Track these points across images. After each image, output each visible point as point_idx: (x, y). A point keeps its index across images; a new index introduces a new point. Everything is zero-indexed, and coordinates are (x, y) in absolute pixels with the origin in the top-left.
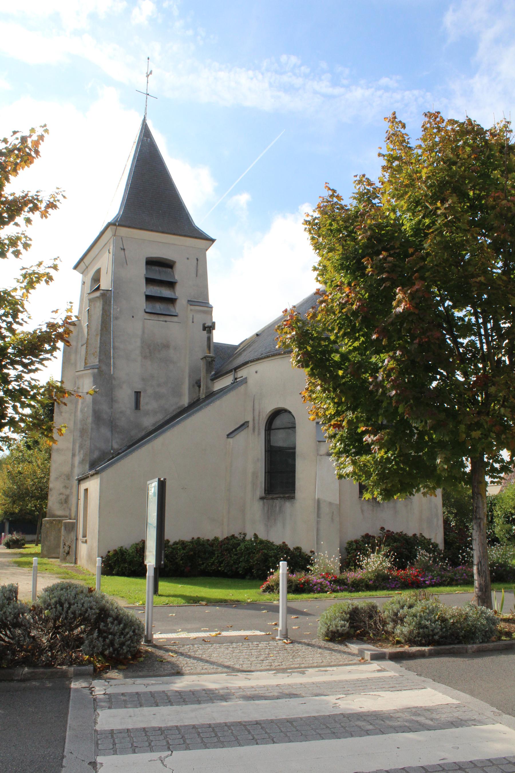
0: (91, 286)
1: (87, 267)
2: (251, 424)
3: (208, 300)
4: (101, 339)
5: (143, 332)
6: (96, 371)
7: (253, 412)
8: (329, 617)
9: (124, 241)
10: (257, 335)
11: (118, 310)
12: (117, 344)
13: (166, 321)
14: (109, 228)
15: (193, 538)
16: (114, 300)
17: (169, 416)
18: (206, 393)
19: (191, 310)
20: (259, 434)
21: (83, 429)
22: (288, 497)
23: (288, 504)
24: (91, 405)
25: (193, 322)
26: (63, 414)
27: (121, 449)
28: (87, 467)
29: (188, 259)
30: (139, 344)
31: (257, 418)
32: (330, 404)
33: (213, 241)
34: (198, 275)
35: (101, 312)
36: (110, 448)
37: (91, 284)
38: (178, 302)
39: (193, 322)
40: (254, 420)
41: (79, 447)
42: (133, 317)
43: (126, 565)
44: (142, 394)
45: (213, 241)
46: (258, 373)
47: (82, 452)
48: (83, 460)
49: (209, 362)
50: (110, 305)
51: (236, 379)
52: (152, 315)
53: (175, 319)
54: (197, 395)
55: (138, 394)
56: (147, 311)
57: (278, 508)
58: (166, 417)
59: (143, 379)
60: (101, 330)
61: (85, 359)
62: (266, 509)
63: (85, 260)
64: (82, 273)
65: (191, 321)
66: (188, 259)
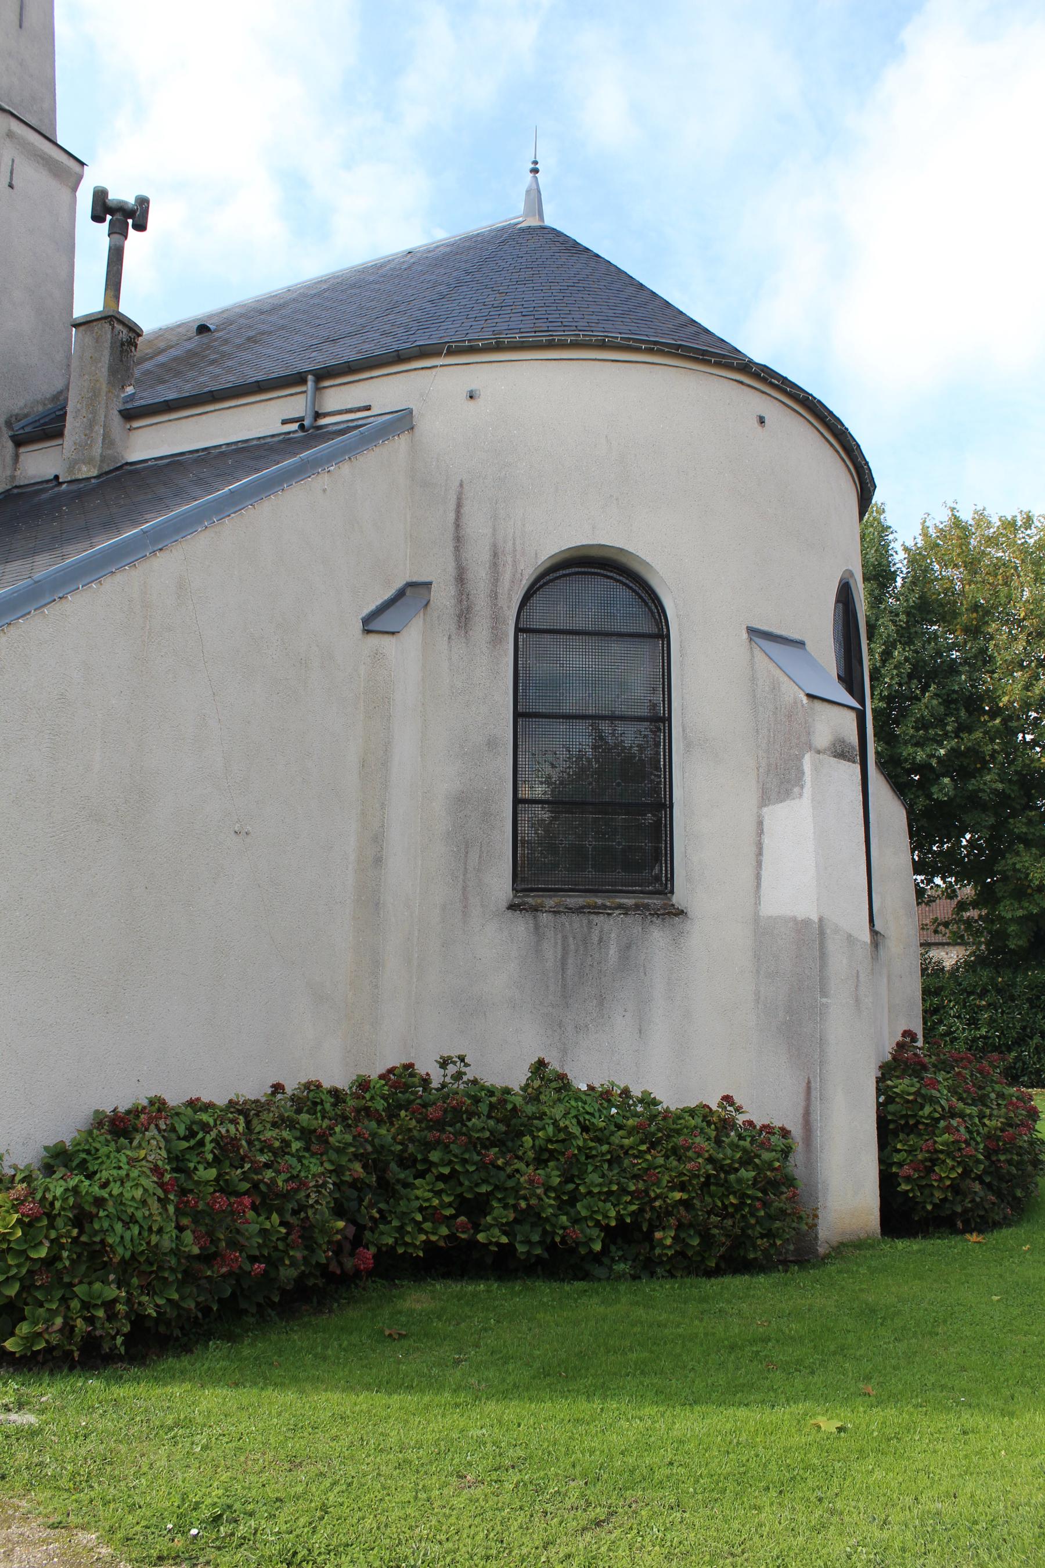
2: (443, 596)
7: (457, 549)
8: (475, 1438)
10: (203, 329)
15: (278, 1088)
18: (103, 458)
19: (10, 135)
20: (496, 639)
22: (637, 907)
23: (658, 936)
25: (11, 186)
31: (479, 575)
34: (25, 24)
40: (461, 578)
43: (112, 1292)
46: (480, 402)
51: (317, 415)
54: (8, 473)
57: (613, 951)
62: (551, 952)
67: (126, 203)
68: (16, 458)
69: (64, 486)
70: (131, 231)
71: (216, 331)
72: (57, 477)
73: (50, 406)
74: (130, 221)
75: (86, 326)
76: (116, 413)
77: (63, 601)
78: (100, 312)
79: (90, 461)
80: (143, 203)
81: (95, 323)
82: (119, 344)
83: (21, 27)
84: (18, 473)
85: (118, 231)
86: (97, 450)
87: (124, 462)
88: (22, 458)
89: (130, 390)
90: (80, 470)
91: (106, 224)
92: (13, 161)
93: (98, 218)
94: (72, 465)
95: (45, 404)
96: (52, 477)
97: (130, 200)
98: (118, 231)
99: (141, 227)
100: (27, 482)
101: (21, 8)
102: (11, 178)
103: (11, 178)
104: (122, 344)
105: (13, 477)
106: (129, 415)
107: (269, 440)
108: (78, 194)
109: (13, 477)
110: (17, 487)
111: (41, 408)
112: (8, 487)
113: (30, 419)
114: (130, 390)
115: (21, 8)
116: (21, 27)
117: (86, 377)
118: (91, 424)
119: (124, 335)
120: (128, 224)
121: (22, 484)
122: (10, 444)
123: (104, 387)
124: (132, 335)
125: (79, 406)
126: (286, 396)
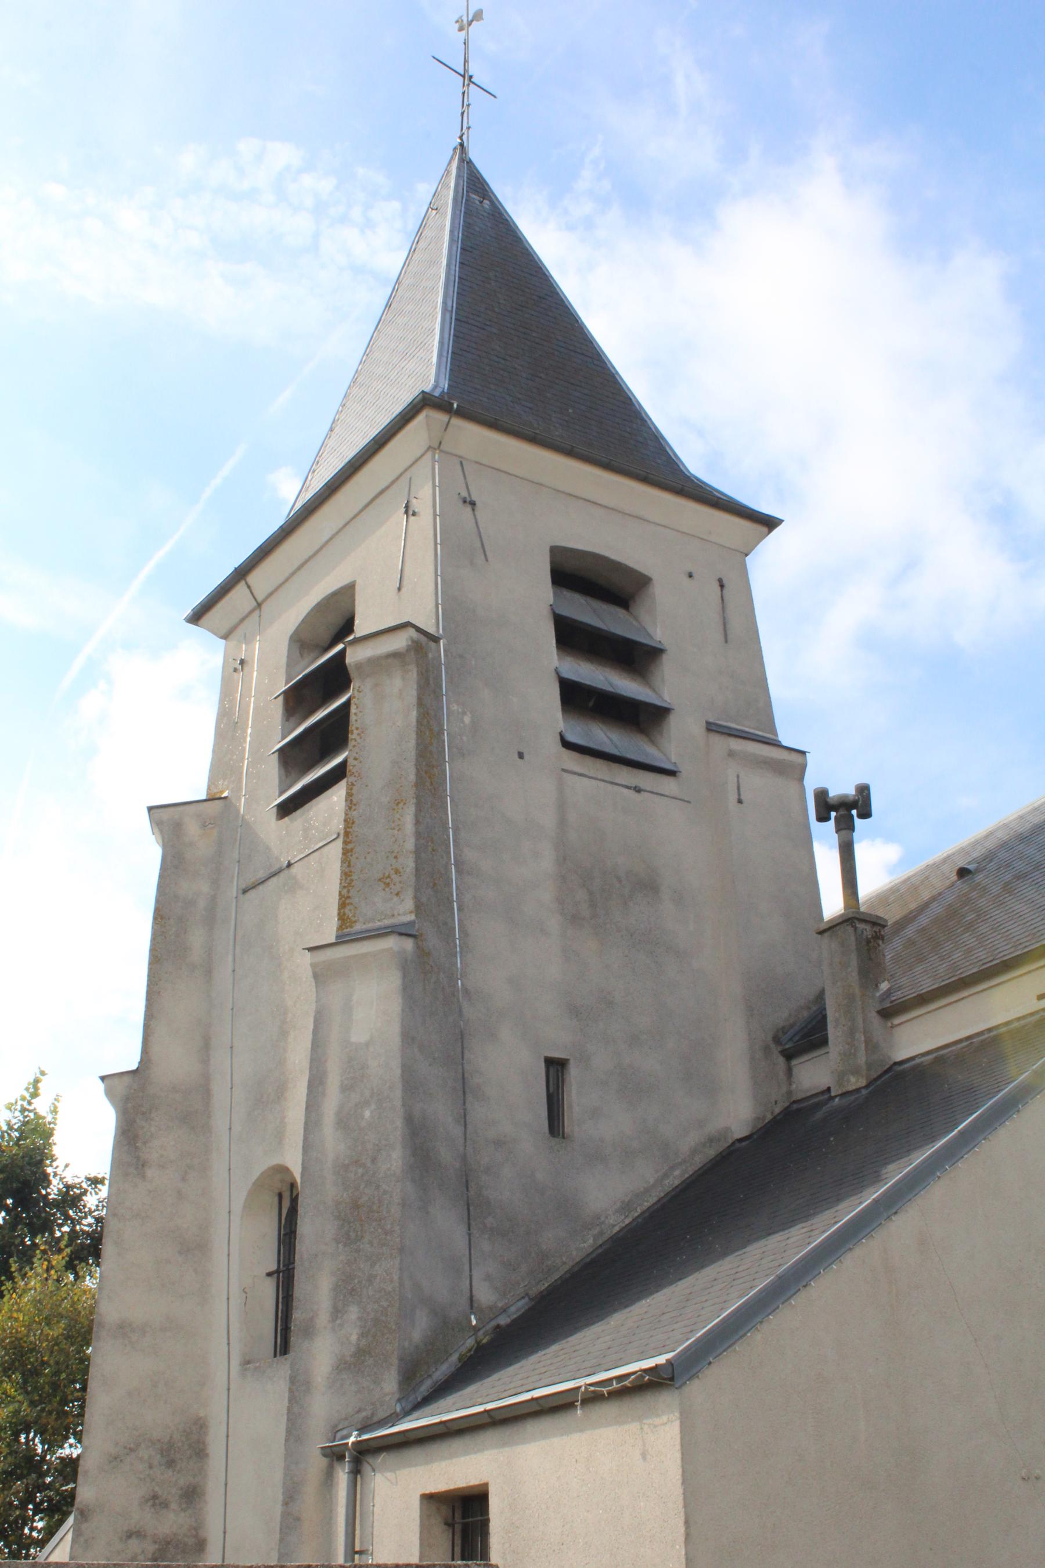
0: (288, 665)
1: (259, 605)
3: (774, 732)
4: (417, 822)
5: (562, 822)
6: (409, 944)
9: (469, 479)
10: (963, 873)
11: (467, 719)
12: (470, 855)
13: (638, 790)
14: (421, 418)
16: (450, 680)
17: (677, 1173)
18: (869, 1066)
19: (731, 754)
21: (356, 1206)
24: (398, 1093)
25: (740, 801)
26: (149, 1173)
27: (504, 1310)
28: (390, 1384)
29: (690, 576)
30: (547, 863)
32: (21, 1403)
33: (770, 523)
34: (730, 637)
35: (414, 714)
36: (464, 1301)
37: (289, 657)
38: (673, 722)
39: (740, 801)
41: (336, 1289)
42: (521, 755)
44: (573, 1073)
45: (770, 523)
47: (353, 1313)
48: (361, 1353)
49: (868, 942)
50: (438, 696)
52: (589, 760)
53: (667, 784)
54: (784, 1089)
55: (556, 1067)
56: (571, 738)
58: (666, 1175)
59: (575, 1011)
60: (416, 785)
61: (343, 904)
63: (253, 578)
64: (225, 637)
65: (733, 798)
66: (690, 576)
67: (846, 796)
68: (789, 1071)
69: (837, 1100)
70: (858, 822)
71: (978, 871)
72: (829, 1089)
73: (814, 1008)
74: (854, 812)
75: (831, 931)
76: (874, 1014)
77: (808, 1288)
78: (841, 916)
79: (856, 1072)
80: (864, 791)
81: (838, 927)
82: (864, 943)
83: (726, 641)
84: (794, 1086)
85: (845, 826)
86: (862, 1059)
87: (891, 1063)
88: (795, 1071)
89: (884, 986)
90: (848, 1081)
91: (832, 822)
92: (738, 777)
93: (822, 818)
94: (841, 1077)
95: (810, 1008)
96: (825, 1088)
97: (850, 791)
98: (845, 826)
99: (866, 814)
100: (803, 1096)
101: (725, 624)
102: (739, 795)
103: (739, 795)
104: (868, 942)
105: (789, 1093)
106: (887, 1014)
107: (1029, 1020)
108: (805, 782)
109: (789, 1093)
110: (794, 1102)
111: (805, 1014)
112: (787, 1104)
113: (796, 1028)
114: (884, 986)
115: (725, 624)
116: (726, 641)
117: (839, 984)
118: (852, 1032)
119: (867, 930)
120: (852, 816)
121: (799, 1098)
122: (781, 1060)
123: (857, 991)
124: (876, 929)
125: (837, 1015)
126: (1037, 969)
